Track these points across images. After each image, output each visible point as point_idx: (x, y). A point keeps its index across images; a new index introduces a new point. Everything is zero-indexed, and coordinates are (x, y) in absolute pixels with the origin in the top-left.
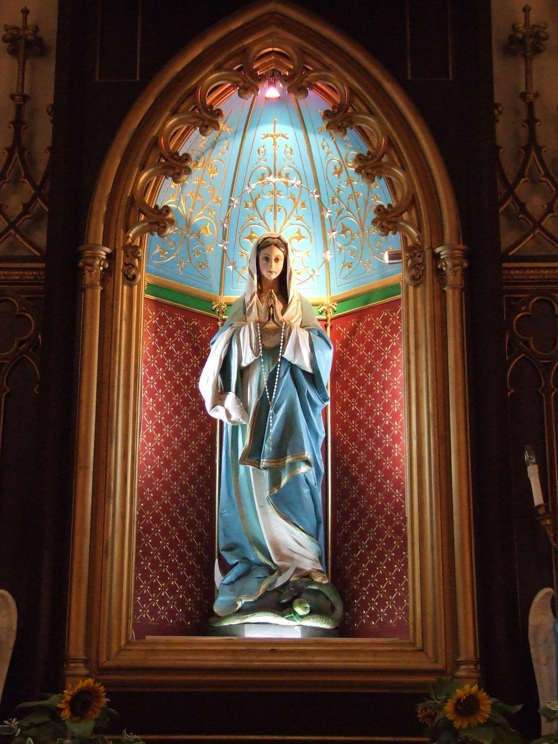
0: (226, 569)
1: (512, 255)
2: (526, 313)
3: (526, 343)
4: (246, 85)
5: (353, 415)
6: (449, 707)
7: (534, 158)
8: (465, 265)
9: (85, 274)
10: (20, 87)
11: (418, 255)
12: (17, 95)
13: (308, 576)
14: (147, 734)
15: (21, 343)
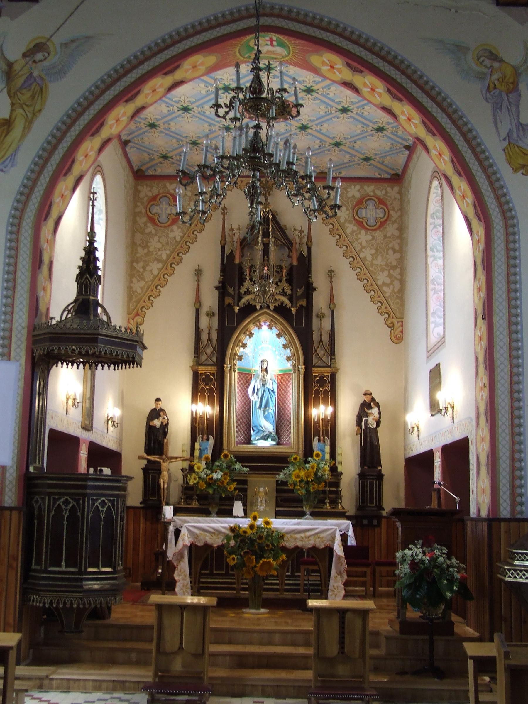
0: (254, 431)
5: (282, 397)
6: (292, 459)
13: (271, 433)
14: (244, 463)
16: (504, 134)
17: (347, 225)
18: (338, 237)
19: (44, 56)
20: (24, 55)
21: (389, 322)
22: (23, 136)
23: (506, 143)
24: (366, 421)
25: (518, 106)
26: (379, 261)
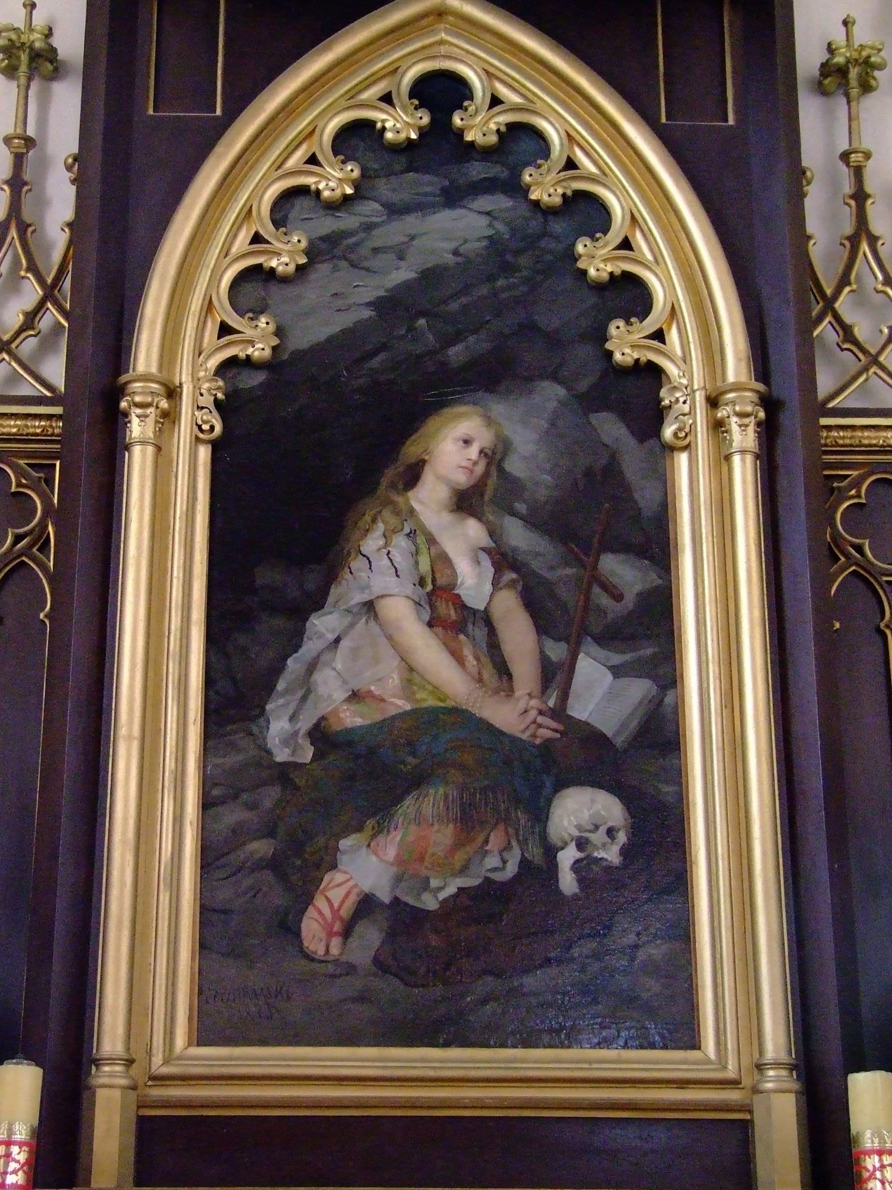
1: (833, 408)
2: (855, 501)
3: (859, 549)
4: (398, 125)
7: (865, 254)
8: (762, 415)
9: (130, 422)
10: (20, 124)
11: (682, 400)
12: (15, 138)
15: (18, 538)
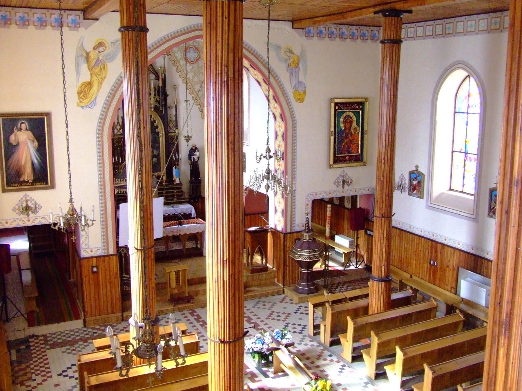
16: (293, 86)
17: (181, 61)
18: (177, 67)
19: (103, 49)
20: (94, 49)
21: (201, 109)
22: (98, 90)
23: (294, 90)
24: (194, 158)
25: (298, 73)
26: (196, 79)
